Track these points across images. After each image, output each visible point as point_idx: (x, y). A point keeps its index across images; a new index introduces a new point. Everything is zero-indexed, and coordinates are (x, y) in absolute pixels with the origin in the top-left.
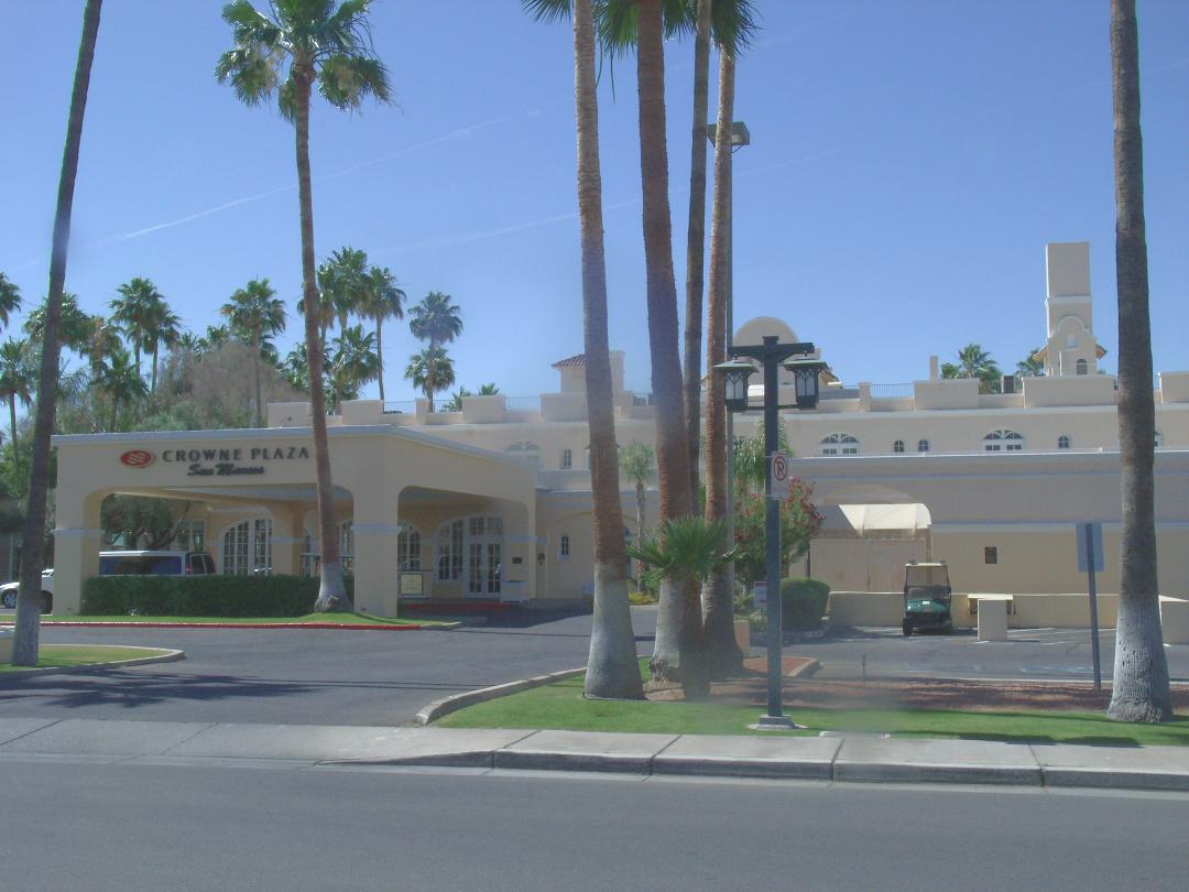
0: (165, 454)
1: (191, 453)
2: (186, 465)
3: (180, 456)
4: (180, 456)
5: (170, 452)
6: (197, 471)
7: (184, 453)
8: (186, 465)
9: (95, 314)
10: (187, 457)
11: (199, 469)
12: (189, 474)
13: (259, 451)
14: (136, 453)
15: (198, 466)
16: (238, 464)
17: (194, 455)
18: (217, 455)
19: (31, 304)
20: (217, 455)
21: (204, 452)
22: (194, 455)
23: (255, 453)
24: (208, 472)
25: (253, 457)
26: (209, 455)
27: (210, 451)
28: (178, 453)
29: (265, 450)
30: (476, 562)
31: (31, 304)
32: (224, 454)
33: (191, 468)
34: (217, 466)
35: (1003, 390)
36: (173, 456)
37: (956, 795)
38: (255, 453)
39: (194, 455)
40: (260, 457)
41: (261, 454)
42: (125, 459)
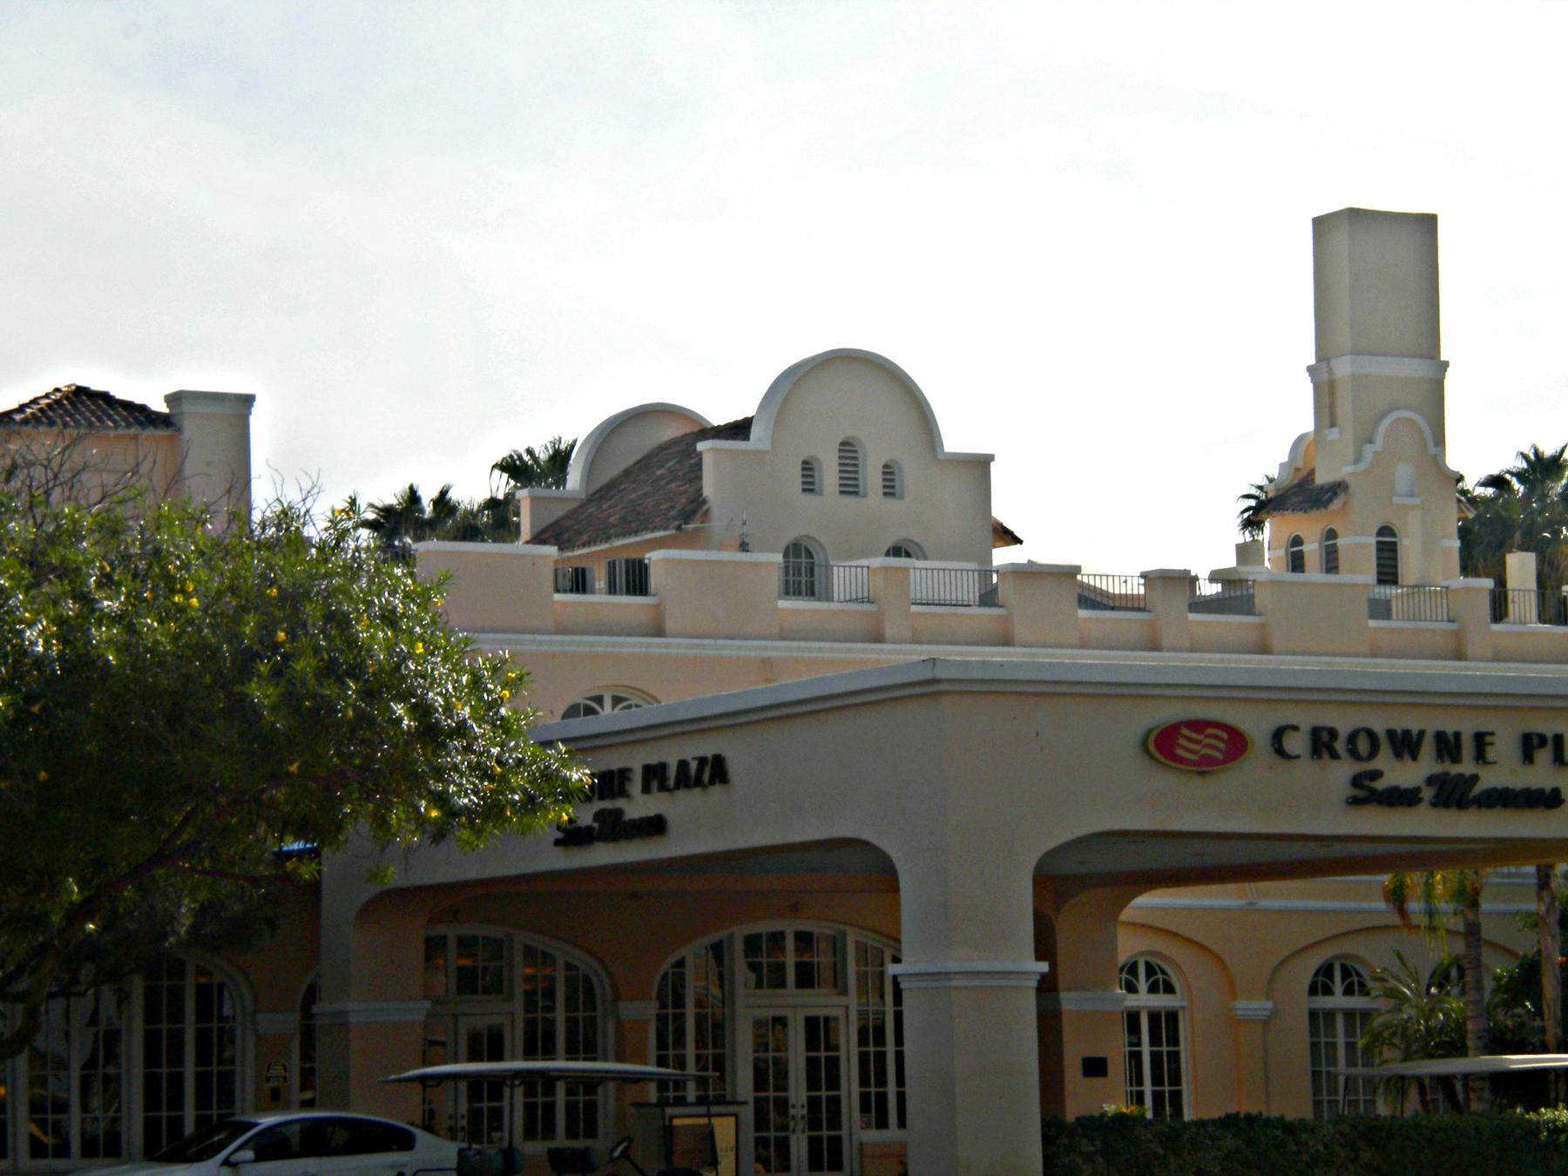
0: (1278, 735)
1: (1353, 737)
2: (1341, 772)
3: (1323, 743)
4: (1323, 743)
5: (1295, 728)
6: (1366, 793)
7: (1333, 733)
8: (1341, 772)
9: (430, 542)
10: (1340, 746)
11: (1380, 785)
12: (1492, 734)
13: (1542, 740)
14: (1198, 725)
15: (1377, 775)
16: (1488, 780)
17: (1363, 746)
18: (1428, 749)
19: (707, 961)
20: (1428, 749)
21: (1391, 734)
22: (1363, 746)
23: (1530, 745)
24: (1403, 798)
25: (1528, 757)
26: (1406, 745)
27: (1407, 733)
28: (1316, 732)
29: (1558, 739)
30: (769, 1074)
31: (707, 961)
32: (1448, 746)
33: (1357, 781)
34: (1431, 781)
35: (671, 1084)
36: (1297, 743)
37: (1489, 1059)
38: (1530, 745)
39: (1364, 743)
40: (1544, 756)
41: (1549, 748)
42: (1385, 530)
